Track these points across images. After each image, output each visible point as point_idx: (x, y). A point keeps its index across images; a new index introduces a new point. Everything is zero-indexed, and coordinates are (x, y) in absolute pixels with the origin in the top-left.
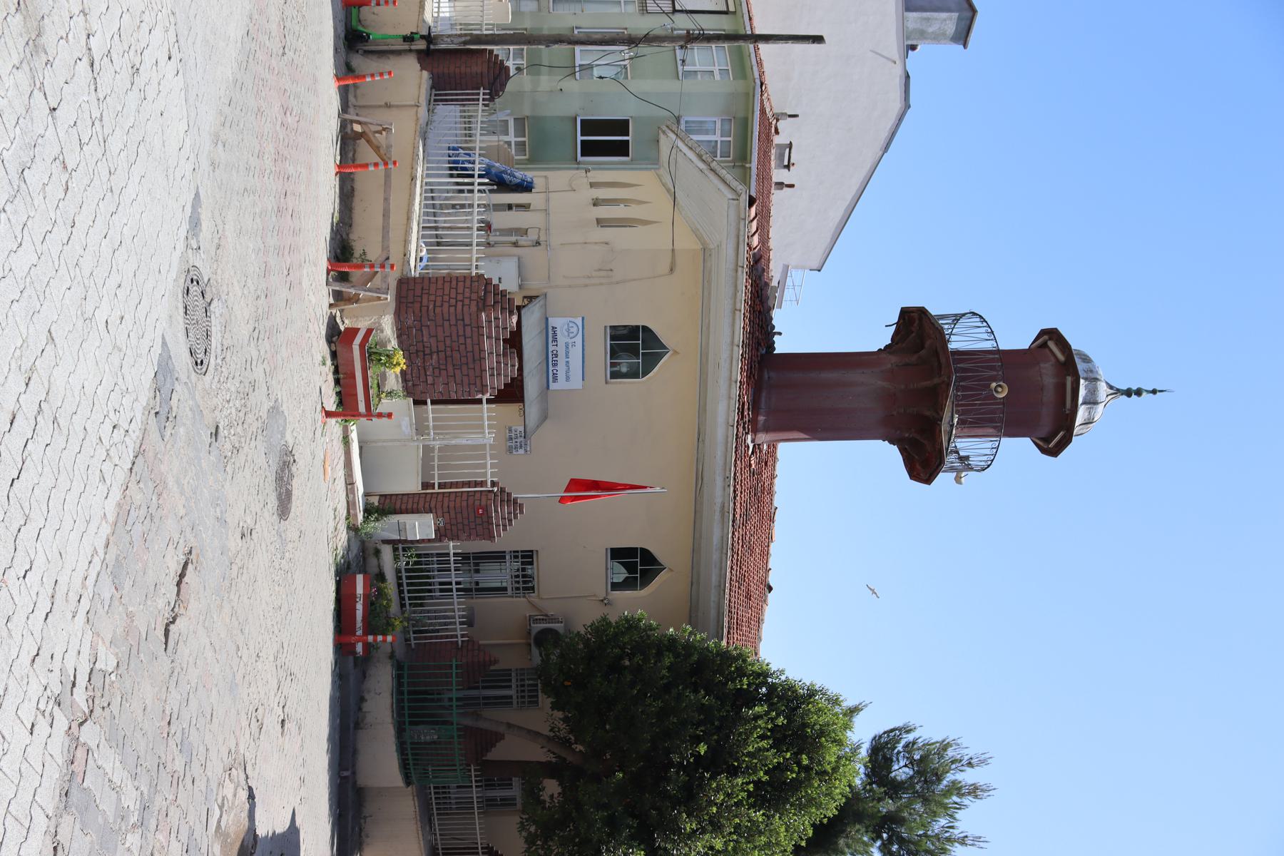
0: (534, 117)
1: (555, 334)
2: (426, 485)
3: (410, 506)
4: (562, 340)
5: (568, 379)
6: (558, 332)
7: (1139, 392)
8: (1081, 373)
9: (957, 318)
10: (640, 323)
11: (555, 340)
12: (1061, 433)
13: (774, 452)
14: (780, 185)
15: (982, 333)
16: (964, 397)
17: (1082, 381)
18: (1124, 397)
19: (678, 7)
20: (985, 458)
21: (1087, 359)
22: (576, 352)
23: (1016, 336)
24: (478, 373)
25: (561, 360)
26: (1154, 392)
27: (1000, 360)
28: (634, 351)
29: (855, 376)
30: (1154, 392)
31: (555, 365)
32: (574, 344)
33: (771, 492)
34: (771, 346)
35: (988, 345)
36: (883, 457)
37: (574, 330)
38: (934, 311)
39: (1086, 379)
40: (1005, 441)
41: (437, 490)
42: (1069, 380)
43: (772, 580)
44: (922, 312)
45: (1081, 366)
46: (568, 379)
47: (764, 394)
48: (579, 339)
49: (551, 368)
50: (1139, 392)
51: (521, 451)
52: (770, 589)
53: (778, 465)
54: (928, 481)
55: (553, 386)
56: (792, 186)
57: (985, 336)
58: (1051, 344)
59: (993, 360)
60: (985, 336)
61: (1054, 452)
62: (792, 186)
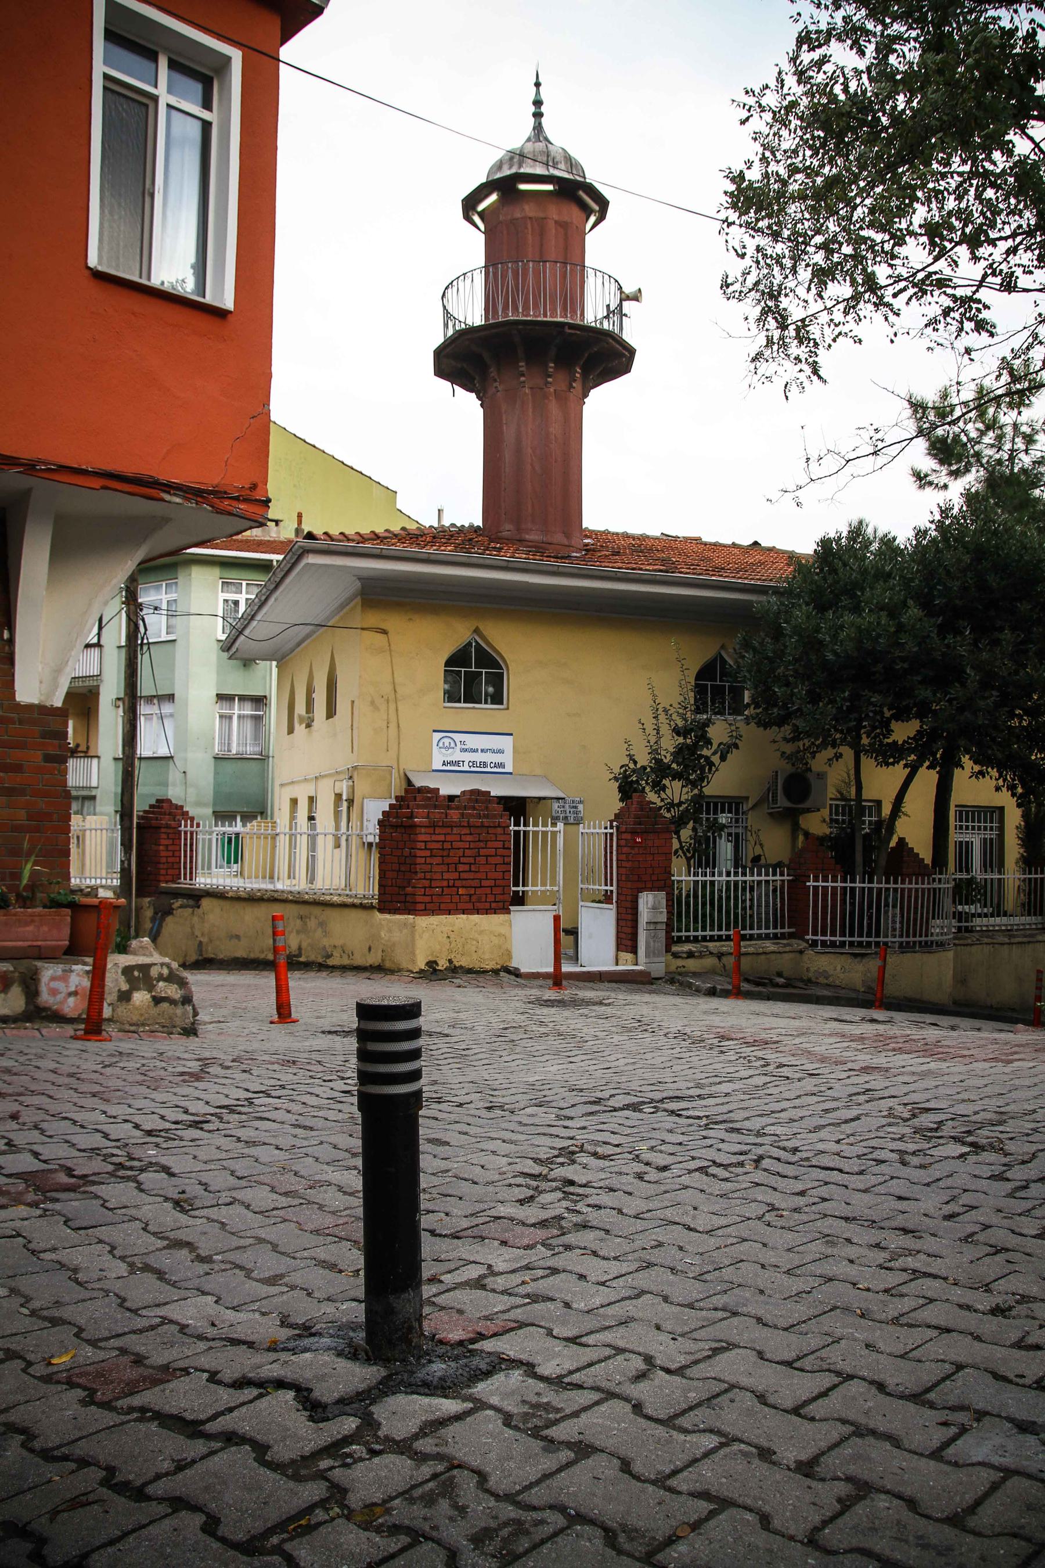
0: (214, 805)
1: (451, 763)
2: (607, 898)
3: (630, 917)
4: (457, 756)
5: (501, 751)
6: (449, 759)
7: (538, 103)
8: (513, 170)
9: (447, 315)
10: (442, 668)
11: (457, 763)
12: (581, 193)
13: (592, 532)
14: (428, 1212)
15: (464, 285)
16: (991, 866)
17: (522, 170)
18: (543, 120)
19: (95, 641)
20: (607, 284)
21: (499, 165)
22: (473, 741)
23: (470, 246)
24: (485, 830)
25: (479, 757)
26: (538, 85)
27: (495, 265)
28: (472, 679)
29: (509, 433)
30: (538, 85)
31: (485, 764)
32: (463, 743)
33: (644, 538)
34: (476, 530)
35: (479, 279)
36: (603, 406)
37: (447, 741)
38: (440, 340)
39: (520, 166)
40: (588, 263)
41: (614, 888)
42: (523, 187)
43: (746, 542)
44: (440, 354)
45: (507, 172)
46: (501, 751)
47: (527, 537)
48: (458, 737)
49: (489, 769)
50: (538, 103)
51: (581, 807)
52: (756, 543)
53: (612, 529)
54: (632, 352)
55: (509, 768)
56: (300, 516)
57: (468, 281)
58: (481, 207)
59: (495, 274)
60: (468, 281)
61: (603, 204)
62: (300, 516)
